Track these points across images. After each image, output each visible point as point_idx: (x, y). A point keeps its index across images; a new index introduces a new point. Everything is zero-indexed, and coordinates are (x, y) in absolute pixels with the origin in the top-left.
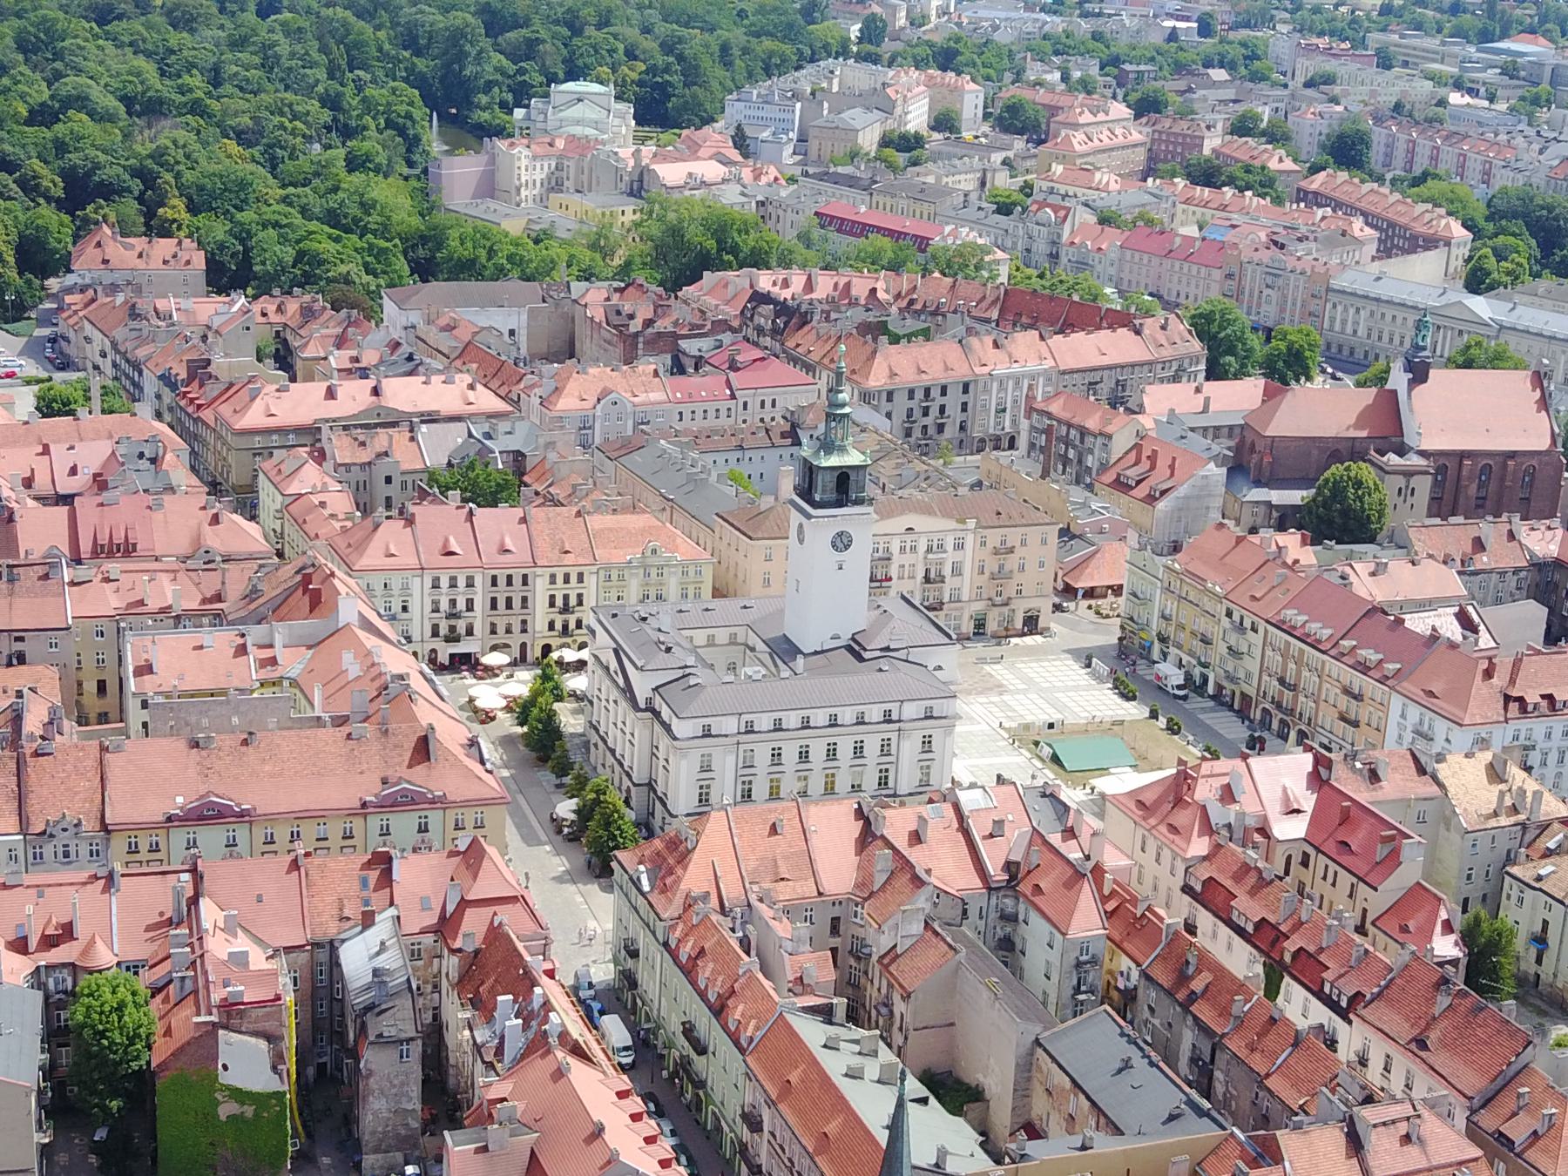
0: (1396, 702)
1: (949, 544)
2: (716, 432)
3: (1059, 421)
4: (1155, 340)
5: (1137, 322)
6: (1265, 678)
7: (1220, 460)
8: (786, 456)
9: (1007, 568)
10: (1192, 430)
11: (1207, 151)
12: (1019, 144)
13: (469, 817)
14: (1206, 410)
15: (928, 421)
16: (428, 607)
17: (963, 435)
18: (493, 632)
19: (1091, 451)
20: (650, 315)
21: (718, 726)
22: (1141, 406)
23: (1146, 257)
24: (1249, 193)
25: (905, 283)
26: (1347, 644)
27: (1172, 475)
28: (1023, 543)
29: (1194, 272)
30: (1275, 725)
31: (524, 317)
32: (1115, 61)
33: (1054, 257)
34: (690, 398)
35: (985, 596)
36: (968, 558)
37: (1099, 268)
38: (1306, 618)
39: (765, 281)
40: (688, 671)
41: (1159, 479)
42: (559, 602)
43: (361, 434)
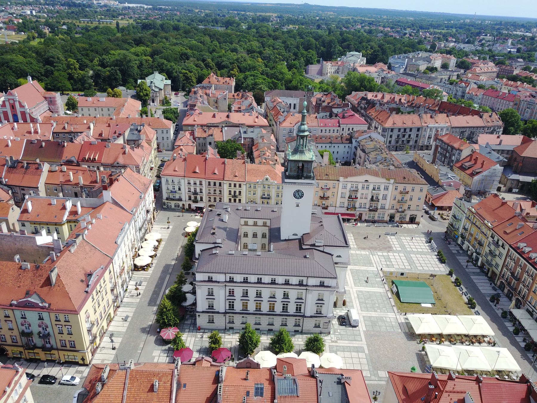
1: (382, 188)
2: (323, 137)
3: (445, 143)
5: (481, 114)
7: (502, 163)
8: (347, 146)
9: (405, 199)
10: (494, 150)
11: (515, 73)
12: (462, 71)
13: (61, 317)
14: (500, 144)
15: (404, 139)
16: (187, 190)
18: (210, 201)
19: (454, 155)
20: (330, 101)
21: (215, 277)
22: (477, 140)
23: (490, 98)
24: (525, 83)
25: (411, 98)
27: (482, 167)
28: (413, 190)
29: (504, 103)
30: (506, 291)
31: (298, 100)
32: (494, 56)
33: (463, 97)
34: (325, 126)
37: (476, 100)
38: (530, 249)
39: (370, 96)
40: (216, 245)
41: (477, 168)
42: (233, 193)
43: (206, 129)
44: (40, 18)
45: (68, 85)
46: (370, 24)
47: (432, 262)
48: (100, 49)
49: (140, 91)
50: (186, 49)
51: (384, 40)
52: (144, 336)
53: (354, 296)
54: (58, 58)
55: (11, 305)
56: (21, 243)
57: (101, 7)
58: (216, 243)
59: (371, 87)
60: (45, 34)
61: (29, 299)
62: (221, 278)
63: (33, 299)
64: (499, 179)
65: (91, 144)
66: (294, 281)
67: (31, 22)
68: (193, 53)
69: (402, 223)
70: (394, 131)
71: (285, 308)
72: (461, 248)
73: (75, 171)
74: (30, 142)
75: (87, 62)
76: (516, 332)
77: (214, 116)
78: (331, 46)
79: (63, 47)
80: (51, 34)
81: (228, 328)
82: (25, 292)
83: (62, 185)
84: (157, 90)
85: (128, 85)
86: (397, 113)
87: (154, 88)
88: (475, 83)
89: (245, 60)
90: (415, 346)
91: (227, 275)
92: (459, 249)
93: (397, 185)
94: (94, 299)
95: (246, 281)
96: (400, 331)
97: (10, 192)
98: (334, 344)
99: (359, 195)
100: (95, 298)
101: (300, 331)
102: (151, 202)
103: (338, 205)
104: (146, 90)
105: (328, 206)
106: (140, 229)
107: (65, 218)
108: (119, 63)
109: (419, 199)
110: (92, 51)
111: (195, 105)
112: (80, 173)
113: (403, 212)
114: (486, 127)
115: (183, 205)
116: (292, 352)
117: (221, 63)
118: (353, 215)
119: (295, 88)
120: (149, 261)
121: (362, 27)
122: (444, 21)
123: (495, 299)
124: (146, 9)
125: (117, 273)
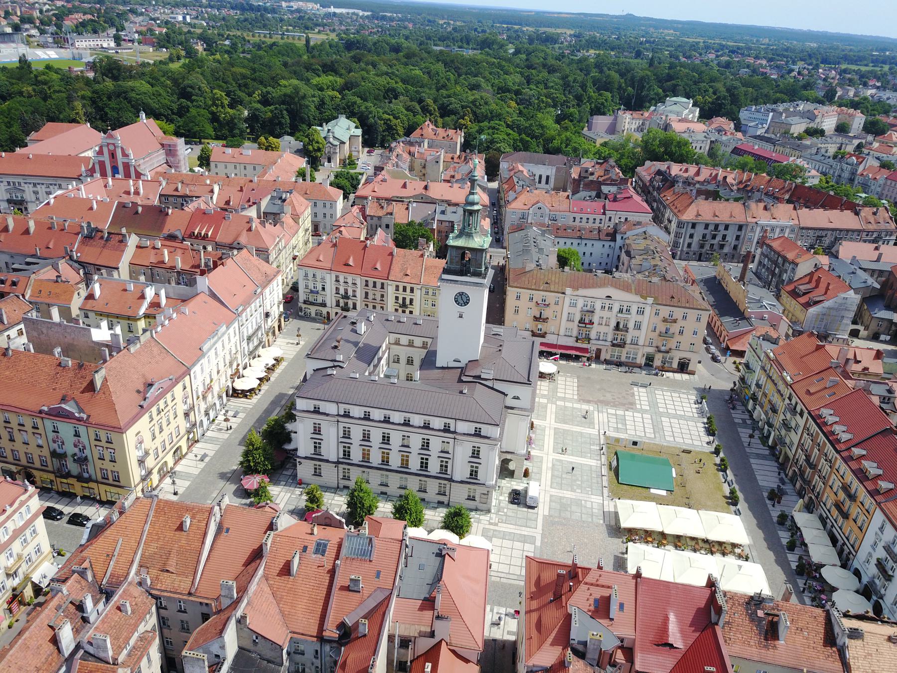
0: (879, 517)
1: (634, 310)
3: (775, 251)
4: (866, 219)
6: (799, 450)
9: (671, 331)
10: (865, 270)
13: (103, 435)
14: (878, 260)
15: (715, 242)
17: (734, 252)
19: (786, 271)
22: (837, 252)
23: (893, 183)
26: (857, 451)
27: (826, 293)
28: (685, 318)
31: (554, 170)
34: (581, 211)
35: (654, 345)
36: (645, 320)
37: (873, 187)
40: (336, 364)
41: (815, 296)
42: (400, 301)
44: (195, 27)
45: (209, 129)
46: (733, 52)
47: (692, 432)
48: (264, 76)
49: (309, 144)
50: (396, 83)
51: (735, 77)
52: (222, 483)
53: (547, 465)
54: (199, 89)
55: (41, 412)
56: (73, 336)
57: (292, 12)
58: (335, 361)
59: (682, 155)
60: (197, 52)
61: (63, 406)
62: (331, 408)
63: (68, 407)
64: (852, 315)
65: (205, 213)
66: (437, 423)
67: (180, 34)
68: (405, 85)
69: (663, 369)
70: (697, 226)
71: (424, 465)
72: (751, 416)
73: (173, 249)
74: (122, 206)
75: (242, 95)
76: (791, 547)
77: (404, 186)
78: (644, 87)
79: (213, 71)
80: (204, 53)
81: (341, 486)
82: (60, 398)
83: (152, 267)
84: (336, 143)
85: (298, 134)
86: (715, 199)
87: (331, 140)
88: (878, 158)
89: (486, 103)
90: (616, 545)
91: (340, 405)
92: (747, 417)
93: (659, 307)
94: (152, 419)
95: (367, 418)
96: (602, 522)
97: (81, 272)
98: (492, 527)
99: (596, 319)
100: (156, 418)
101: (446, 502)
102: (276, 303)
103: (562, 332)
104: (317, 142)
105: (546, 333)
106: (249, 339)
107: (142, 311)
108: (288, 99)
109: (695, 333)
110: (254, 80)
111: (383, 169)
112: (179, 251)
113: (668, 352)
114: (864, 231)
115: (328, 313)
116: (421, 528)
117: (448, 106)
118: (586, 350)
119: (557, 151)
120: (255, 384)
121: (717, 56)
122: (872, 50)
123: (775, 496)
124: (362, 17)
125: (197, 392)
